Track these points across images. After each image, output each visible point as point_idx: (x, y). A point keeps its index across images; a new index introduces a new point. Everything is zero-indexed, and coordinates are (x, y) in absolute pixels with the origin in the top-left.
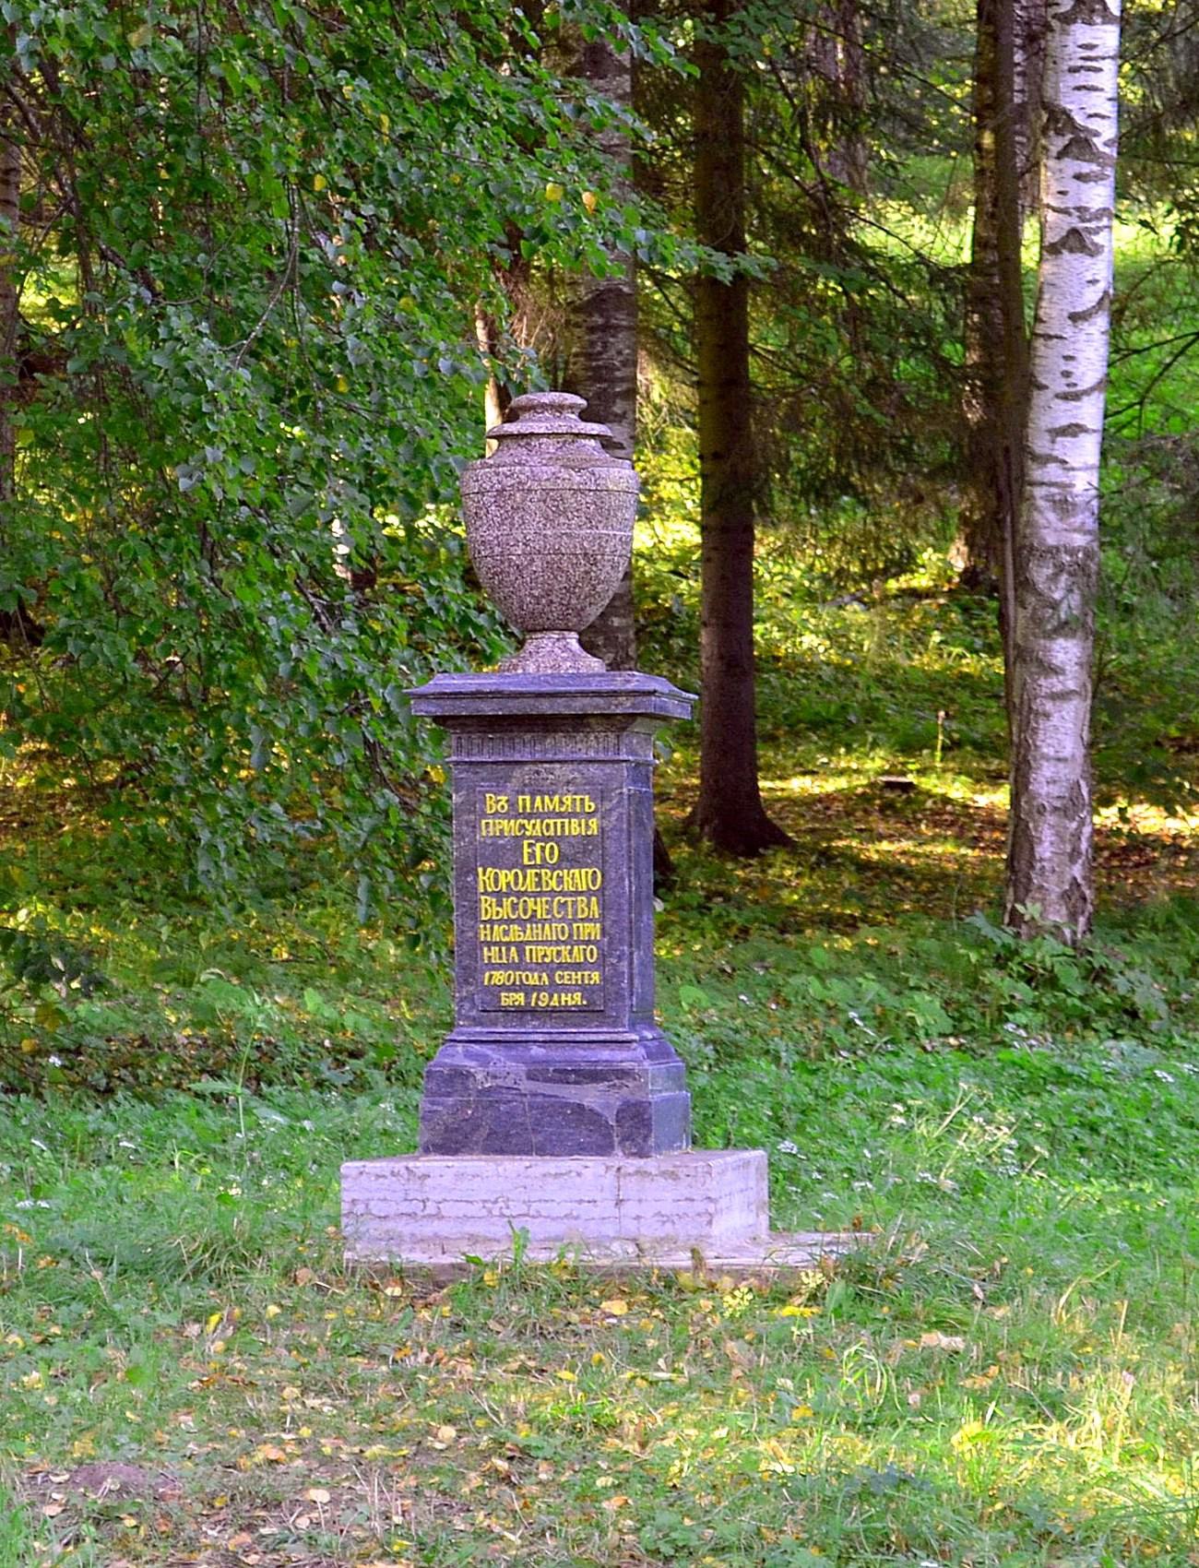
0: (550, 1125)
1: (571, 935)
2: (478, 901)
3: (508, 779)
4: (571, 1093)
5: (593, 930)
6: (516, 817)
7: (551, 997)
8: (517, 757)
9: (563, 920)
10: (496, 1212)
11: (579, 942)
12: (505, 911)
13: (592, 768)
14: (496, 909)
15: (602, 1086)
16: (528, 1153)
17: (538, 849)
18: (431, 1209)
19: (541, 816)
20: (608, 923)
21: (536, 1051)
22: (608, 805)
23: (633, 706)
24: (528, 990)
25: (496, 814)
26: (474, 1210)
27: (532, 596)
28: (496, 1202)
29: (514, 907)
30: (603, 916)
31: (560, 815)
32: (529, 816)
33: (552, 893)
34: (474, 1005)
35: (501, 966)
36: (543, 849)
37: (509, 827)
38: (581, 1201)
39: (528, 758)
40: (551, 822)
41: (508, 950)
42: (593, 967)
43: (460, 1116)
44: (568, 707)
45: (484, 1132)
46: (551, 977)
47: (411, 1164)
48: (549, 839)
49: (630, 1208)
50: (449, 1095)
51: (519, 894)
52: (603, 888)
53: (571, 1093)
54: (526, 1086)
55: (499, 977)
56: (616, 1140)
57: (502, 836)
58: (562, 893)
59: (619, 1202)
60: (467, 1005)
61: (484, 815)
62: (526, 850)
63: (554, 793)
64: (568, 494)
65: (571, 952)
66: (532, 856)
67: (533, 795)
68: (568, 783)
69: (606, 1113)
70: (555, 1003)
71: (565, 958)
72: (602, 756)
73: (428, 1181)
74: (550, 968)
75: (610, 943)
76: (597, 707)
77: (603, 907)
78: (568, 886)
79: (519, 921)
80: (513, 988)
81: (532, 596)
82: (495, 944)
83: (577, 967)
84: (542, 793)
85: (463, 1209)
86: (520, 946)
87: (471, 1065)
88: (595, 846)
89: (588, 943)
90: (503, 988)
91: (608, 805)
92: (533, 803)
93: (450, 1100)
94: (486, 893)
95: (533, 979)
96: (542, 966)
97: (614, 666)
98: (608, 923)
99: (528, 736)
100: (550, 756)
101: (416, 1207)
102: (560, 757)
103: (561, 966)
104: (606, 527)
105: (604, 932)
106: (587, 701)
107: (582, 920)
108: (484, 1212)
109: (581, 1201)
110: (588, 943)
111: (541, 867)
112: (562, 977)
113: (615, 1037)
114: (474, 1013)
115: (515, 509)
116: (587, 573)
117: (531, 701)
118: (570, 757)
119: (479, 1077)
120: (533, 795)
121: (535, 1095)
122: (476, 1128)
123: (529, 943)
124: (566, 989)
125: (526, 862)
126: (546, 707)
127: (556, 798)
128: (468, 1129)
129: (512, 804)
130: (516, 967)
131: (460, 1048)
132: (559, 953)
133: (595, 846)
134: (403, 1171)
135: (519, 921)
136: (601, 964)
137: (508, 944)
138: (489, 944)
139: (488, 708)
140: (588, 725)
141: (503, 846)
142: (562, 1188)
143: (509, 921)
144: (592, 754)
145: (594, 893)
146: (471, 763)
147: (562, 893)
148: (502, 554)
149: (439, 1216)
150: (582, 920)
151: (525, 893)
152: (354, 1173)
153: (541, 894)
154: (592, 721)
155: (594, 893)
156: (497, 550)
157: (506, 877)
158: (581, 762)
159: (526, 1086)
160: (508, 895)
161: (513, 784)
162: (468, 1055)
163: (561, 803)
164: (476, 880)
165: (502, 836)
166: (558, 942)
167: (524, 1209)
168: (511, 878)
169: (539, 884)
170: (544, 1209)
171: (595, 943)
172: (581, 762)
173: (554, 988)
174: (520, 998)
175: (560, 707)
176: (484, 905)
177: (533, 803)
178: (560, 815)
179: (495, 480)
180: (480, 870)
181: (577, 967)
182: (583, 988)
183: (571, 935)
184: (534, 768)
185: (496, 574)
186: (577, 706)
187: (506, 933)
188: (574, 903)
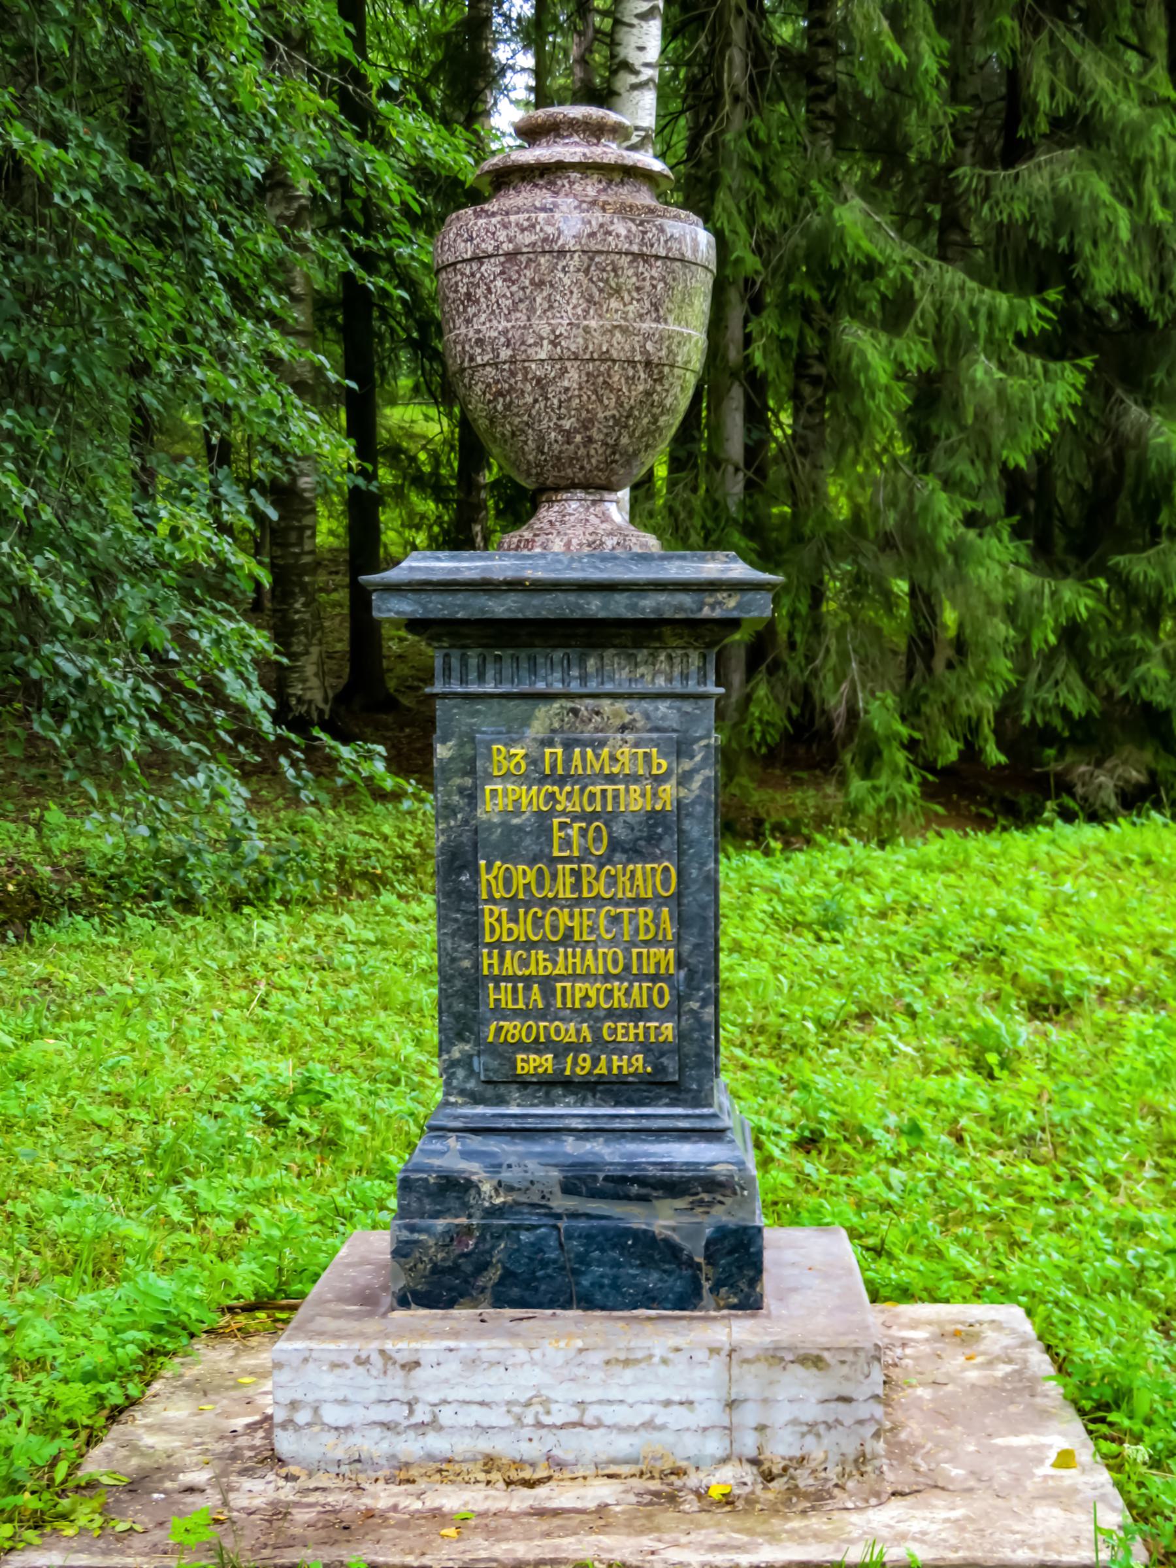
0: (600, 1263)
1: (627, 968)
2: (478, 913)
3: (526, 722)
4: (635, 1217)
5: (664, 957)
6: (543, 779)
7: (596, 1061)
8: (541, 686)
9: (613, 942)
10: (529, 1420)
11: (641, 977)
12: (523, 929)
13: (663, 707)
14: (506, 925)
15: (681, 1203)
16: (566, 1305)
17: (574, 832)
18: (422, 1414)
19: (583, 781)
20: (686, 948)
21: (571, 1147)
22: (687, 765)
23: (738, 607)
24: (560, 1051)
25: (507, 776)
26: (495, 1417)
27: (559, 429)
28: (528, 1404)
29: (537, 923)
30: (679, 937)
31: (611, 779)
32: (561, 781)
33: (598, 901)
34: (471, 1073)
35: (517, 1014)
36: (583, 833)
37: (532, 798)
38: (667, 1403)
39: (558, 687)
40: (597, 789)
41: (527, 988)
42: (664, 1015)
43: (456, 1249)
44: (633, 607)
45: (493, 1275)
46: (596, 1032)
47: (389, 1345)
48: (595, 816)
49: (749, 1415)
50: (436, 1215)
51: (545, 903)
52: (679, 895)
53: (635, 1217)
54: (561, 1203)
55: (514, 1029)
56: (707, 1285)
57: (517, 812)
58: (616, 902)
59: (731, 1405)
60: (461, 1073)
61: (490, 778)
62: (557, 834)
63: (602, 744)
64: (624, 261)
65: (628, 993)
66: (567, 843)
67: (568, 746)
68: (623, 728)
69: (687, 1246)
70: (602, 1069)
71: (619, 1000)
72: (677, 687)
73: (418, 1372)
74: (592, 1016)
75: (691, 974)
76: (680, 608)
77: (681, 921)
78: (624, 891)
79: (545, 944)
80: (537, 1047)
81: (559, 429)
82: (507, 979)
83: (637, 1015)
84: (583, 744)
85: (477, 1415)
86: (547, 984)
87: (474, 1169)
88: (667, 829)
89: (654, 978)
90: (520, 1046)
91: (687, 765)
92: (568, 760)
93: (440, 1224)
94: (491, 900)
95: (568, 1032)
96: (582, 1013)
97: (277, 652)
98: (686, 948)
99: (558, 654)
100: (593, 686)
101: (396, 1413)
102: (609, 687)
103: (612, 1014)
104: (678, 320)
105: (680, 962)
106: (663, 598)
107: (646, 943)
108: (509, 1421)
109: (667, 1403)
110: (654, 978)
111: (581, 860)
112: (614, 1031)
113: (698, 1124)
114: (471, 1085)
115: (539, 285)
116: (648, 394)
117: (572, 598)
118: (625, 689)
119: (486, 1188)
120: (568, 746)
121: (574, 1215)
122: (482, 1267)
123: (561, 978)
124: (618, 1048)
125: (556, 853)
126: (594, 606)
127: (605, 752)
128: (468, 1268)
129: (534, 761)
130: (542, 1015)
131: (453, 1142)
132: (609, 994)
133: (667, 829)
134: (376, 1358)
135: (545, 944)
136: (676, 1011)
137: (528, 980)
138: (497, 980)
139: (501, 607)
140: (659, 638)
141: (519, 828)
142: (637, 1383)
143: (529, 945)
144: (661, 683)
145: (665, 901)
146: (467, 696)
147: (616, 902)
148: (512, 361)
149: (433, 1425)
150: (646, 943)
151: (554, 901)
152: (296, 1360)
153: (579, 902)
154: (667, 631)
155: (665, 901)
156: (505, 354)
157: (524, 875)
158: (643, 696)
159: (561, 1203)
160: (528, 905)
161: (537, 729)
162: (467, 1155)
163: (613, 759)
164: (476, 882)
165: (517, 812)
166: (607, 977)
167: (574, 1415)
168: (531, 876)
169: (577, 887)
170: (610, 1415)
171: (668, 978)
172: (643, 696)
173: (600, 1045)
174: (546, 1063)
175: (619, 606)
176: (487, 920)
177: (568, 760)
178: (611, 779)
179: (502, 235)
180: (483, 863)
181: (637, 1015)
182: (646, 1048)
183: (627, 968)
184: (570, 705)
185: (500, 393)
186: (649, 605)
187: (525, 963)
188: (634, 916)
